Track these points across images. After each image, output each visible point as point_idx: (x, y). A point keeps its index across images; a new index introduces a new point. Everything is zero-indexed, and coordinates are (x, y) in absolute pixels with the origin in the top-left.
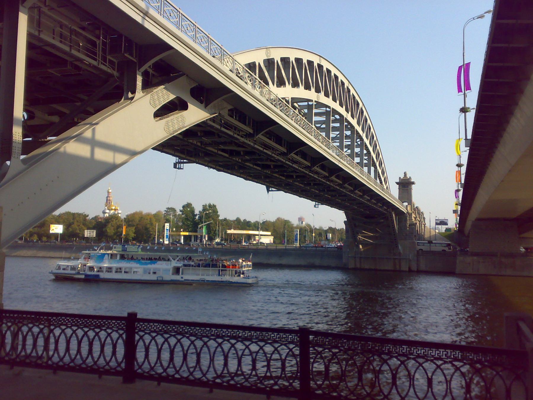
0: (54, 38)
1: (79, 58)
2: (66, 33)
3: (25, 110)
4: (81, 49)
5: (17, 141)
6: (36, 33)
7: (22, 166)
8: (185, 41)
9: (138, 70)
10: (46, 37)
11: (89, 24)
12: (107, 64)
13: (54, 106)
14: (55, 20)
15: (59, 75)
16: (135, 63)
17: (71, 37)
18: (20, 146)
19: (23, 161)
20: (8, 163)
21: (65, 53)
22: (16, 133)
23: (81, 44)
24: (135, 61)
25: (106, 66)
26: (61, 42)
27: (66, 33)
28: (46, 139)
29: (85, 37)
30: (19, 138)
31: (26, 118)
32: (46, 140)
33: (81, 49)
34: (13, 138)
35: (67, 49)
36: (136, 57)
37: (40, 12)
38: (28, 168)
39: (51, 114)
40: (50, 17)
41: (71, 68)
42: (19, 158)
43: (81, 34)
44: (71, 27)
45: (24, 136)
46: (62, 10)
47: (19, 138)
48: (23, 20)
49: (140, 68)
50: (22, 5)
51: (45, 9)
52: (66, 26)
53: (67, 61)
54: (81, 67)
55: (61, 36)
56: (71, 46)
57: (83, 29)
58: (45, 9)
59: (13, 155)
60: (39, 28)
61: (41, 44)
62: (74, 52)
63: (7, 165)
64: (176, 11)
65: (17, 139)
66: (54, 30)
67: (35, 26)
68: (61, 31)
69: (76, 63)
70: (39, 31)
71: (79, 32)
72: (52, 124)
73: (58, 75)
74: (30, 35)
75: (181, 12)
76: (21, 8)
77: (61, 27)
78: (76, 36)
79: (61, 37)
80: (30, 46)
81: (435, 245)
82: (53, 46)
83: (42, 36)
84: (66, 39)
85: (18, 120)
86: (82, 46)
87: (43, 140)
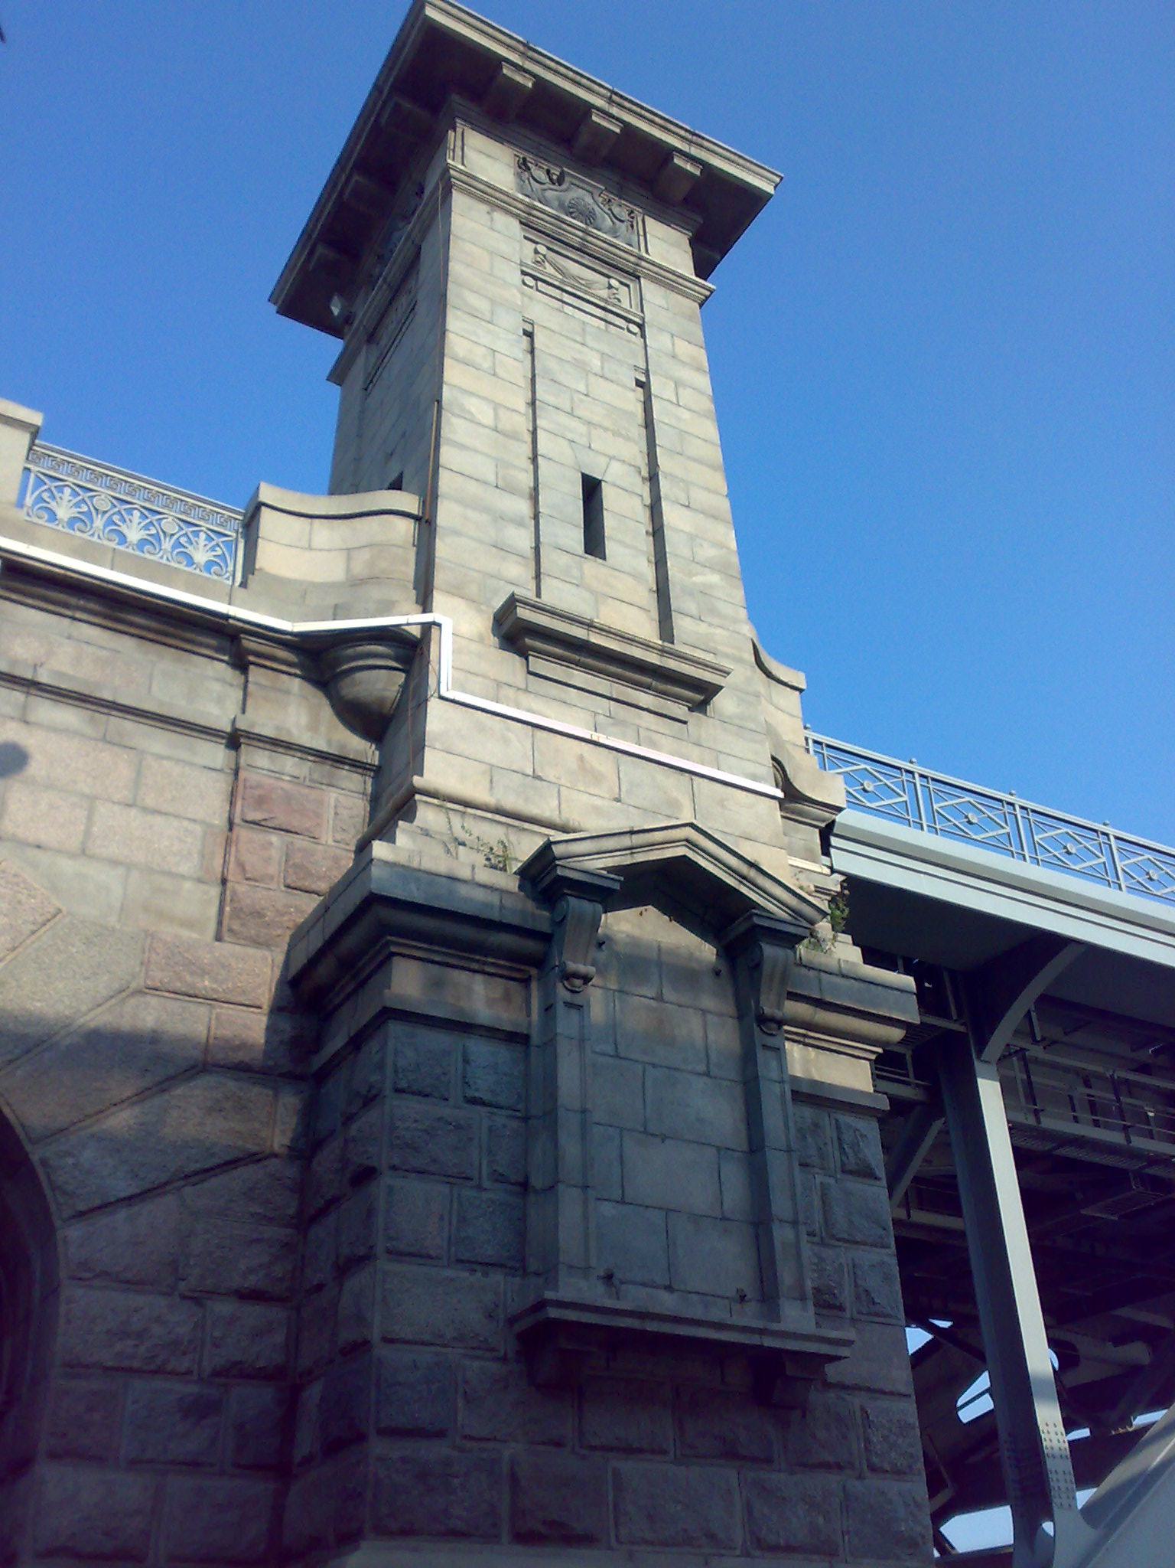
0: (1076, 1120)
1: (1157, 1154)
2: (1103, 1094)
3: (1053, 1343)
4: (1155, 1130)
5: (1056, 1451)
6: (1031, 1121)
7: (1087, 1534)
8: (921, 848)
9: (980, 1052)
10: (1056, 1122)
11: (1156, 1053)
12: (911, 1079)
13: (1125, 1312)
14: (1067, 1069)
15: (1115, 1218)
16: (967, 1034)
17: (1118, 1100)
18: (1068, 1465)
19: (1090, 1512)
20: (1048, 1527)
21: (1112, 1149)
22: (1047, 1425)
23: (1151, 1114)
24: (962, 1029)
25: (907, 1084)
26: (1096, 1124)
27: (1103, 1094)
28: (1131, 1425)
29: (1158, 1091)
30: (1059, 1441)
31: (1056, 1365)
32: (1130, 1430)
33: (1155, 1130)
34: (1044, 1443)
35: (1116, 1138)
36: (960, 1014)
37: (1026, 1062)
38: (1106, 1537)
39: (1120, 1340)
40: (1054, 1066)
41: (1141, 1189)
42: (1072, 1505)
43: (1145, 1087)
44: (1112, 1077)
45: (1069, 1425)
46: (1078, 1038)
47: (1059, 1441)
48: (990, 1094)
49: (982, 1044)
50: (979, 1058)
51: (1036, 1051)
52: (1100, 1077)
53: (1124, 1172)
54: (1169, 1179)
55: (1093, 1107)
56: (1125, 1128)
57: (1144, 1069)
58: (1036, 1051)
59: (1056, 1501)
60: (1074, 1110)
61: (1048, 1146)
62: (1139, 1142)
63: (1048, 1535)
64: (1093, 835)
65: (1055, 1443)
66: (1071, 1098)
67: (1023, 1100)
68: (1089, 1095)
69: (1150, 1171)
70: (1036, 1113)
71: (1137, 1084)
72: (1135, 1370)
73: (1112, 1218)
74: (1014, 1129)
75: (1018, 801)
76: (978, 1066)
77: (1087, 1084)
78: (1131, 1094)
79: (1093, 1112)
80: (1022, 1158)
81: (609, 94)
82: (1079, 1142)
83: (1048, 1123)
84: (1107, 1114)
85: (1042, 1381)
86: (1155, 1117)
87: (1121, 1431)
